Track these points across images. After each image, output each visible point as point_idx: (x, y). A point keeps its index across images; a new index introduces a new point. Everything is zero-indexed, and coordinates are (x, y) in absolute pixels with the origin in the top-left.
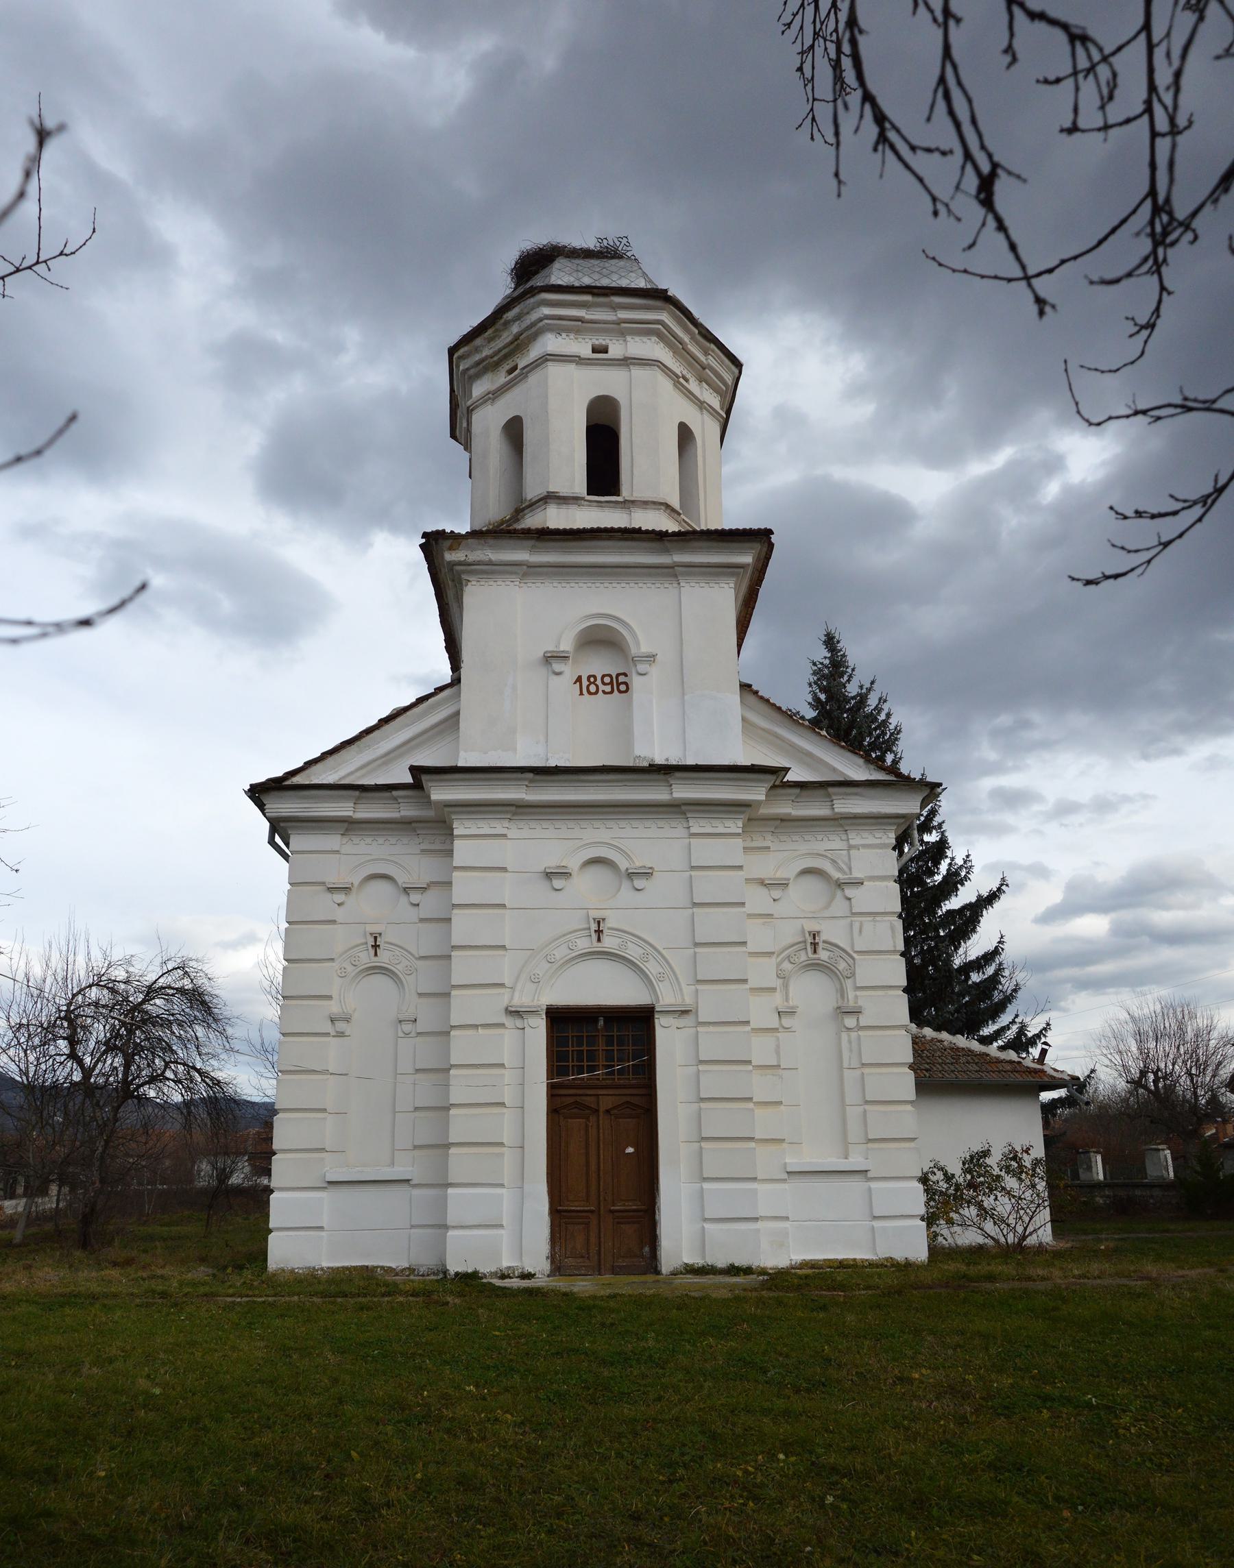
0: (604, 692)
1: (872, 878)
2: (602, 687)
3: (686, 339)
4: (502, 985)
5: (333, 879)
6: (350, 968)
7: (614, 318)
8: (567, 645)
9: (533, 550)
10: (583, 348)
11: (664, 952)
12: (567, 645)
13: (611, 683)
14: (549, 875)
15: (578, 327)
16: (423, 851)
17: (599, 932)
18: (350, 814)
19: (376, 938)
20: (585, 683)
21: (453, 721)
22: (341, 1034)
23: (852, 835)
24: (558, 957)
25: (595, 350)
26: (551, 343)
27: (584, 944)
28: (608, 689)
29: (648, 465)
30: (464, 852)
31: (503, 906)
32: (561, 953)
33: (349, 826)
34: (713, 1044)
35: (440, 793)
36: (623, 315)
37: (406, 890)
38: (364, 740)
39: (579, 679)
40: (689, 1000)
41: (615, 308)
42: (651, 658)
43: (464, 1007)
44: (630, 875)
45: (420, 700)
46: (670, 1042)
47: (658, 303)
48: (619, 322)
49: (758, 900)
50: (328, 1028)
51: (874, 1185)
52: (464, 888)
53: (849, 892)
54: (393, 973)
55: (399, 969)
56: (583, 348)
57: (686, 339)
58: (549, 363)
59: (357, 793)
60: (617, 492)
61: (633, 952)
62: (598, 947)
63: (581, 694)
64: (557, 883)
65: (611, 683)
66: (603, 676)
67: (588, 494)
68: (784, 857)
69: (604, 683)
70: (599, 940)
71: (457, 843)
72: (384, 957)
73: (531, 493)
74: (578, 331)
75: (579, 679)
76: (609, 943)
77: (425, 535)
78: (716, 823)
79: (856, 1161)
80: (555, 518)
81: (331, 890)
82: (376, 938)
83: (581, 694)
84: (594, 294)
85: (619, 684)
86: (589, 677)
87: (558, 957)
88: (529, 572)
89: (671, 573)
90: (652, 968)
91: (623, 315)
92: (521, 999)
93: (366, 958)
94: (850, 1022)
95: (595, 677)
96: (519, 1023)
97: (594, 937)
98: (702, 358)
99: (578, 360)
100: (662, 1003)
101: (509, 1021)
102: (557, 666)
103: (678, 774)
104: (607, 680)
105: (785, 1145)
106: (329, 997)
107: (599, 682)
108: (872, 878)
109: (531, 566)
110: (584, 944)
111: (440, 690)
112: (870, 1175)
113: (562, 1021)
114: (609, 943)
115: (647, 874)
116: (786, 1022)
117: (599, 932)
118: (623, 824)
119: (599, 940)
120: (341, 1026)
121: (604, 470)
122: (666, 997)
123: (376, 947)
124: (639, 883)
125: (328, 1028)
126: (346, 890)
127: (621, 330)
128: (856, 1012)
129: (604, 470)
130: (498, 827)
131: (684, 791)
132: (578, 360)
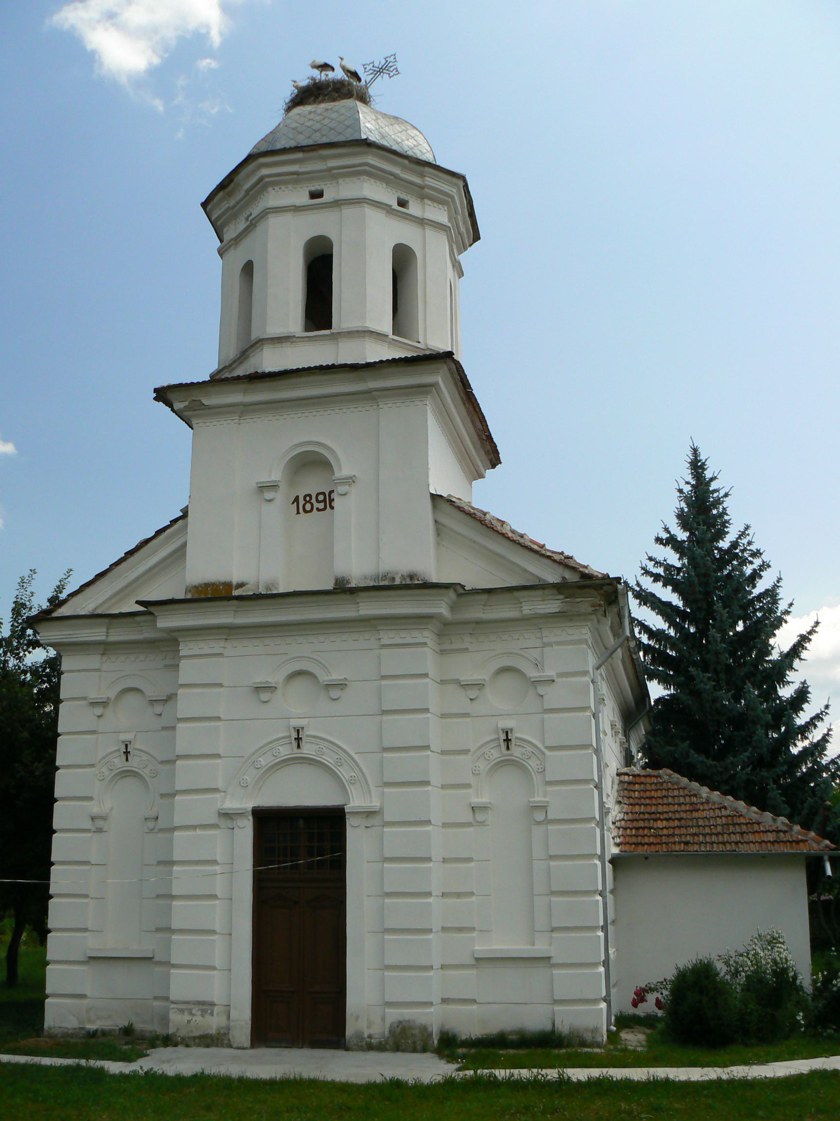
0: (318, 510)
2: (316, 505)
3: (397, 170)
4: (215, 790)
5: (93, 695)
6: (107, 772)
7: (324, 167)
8: (276, 475)
9: (245, 392)
10: (301, 197)
11: (356, 757)
12: (276, 475)
13: (324, 501)
14: (259, 689)
15: (297, 178)
16: (165, 666)
17: (298, 739)
18: (103, 638)
19: (126, 745)
20: (302, 502)
21: (181, 552)
22: (100, 830)
23: (545, 633)
24: (263, 763)
25: (316, 195)
26: (274, 198)
27: (286, 751)
28: (321, 506)
29: (363, 296)
30: (188, 670)
31: (218, 719)
32: (265, 761)
33: (106, 648)
34: (396, 840)
35: (166, 621)
36: (332, 163)
37: (152, 702)
38: (113, 572)
39: (297, 499)
40: (375, 804)
41: (325, 158)
42: (350, 480)
43: (186, 808)
44: (329, 686)
45: (159, 533)
46: (359, 843)
47: (365, 149)
48: (330, 169)
49: (459, 701)
50: (88, 824)
51: (556, 972)
52: (188, 703)
53: (541, 690)
54: (142, 776)
55: (146, 773)
56: (301, 197)
57: (397, 170)
58: (270, 215)
59: (106, 620)
60: (329, 326)
61: (328, 759)
62: (297, 753)
63: (298, 513)
64: (264, 696)
65: (324, 501)
66: (318, 495)
67: (307, 329)
68: (476, 662)
69: (318, 501)
70: (299, 747)
71: (183, 663)
72: (135, 763)
73: (254, 336)
74: (296, 182)
75: (297, 499)
76: (308, 749)
77: (156, 390)
78: (403, 634)
79: (541, 947)
80: (270, 361)
81: (94, 704)
82: (126, 745)
83: (298, 513)
84: (303, 151)
85: (327, 501)
86: (305, 497)
87: (263, 763)
88: (245, 410)
89: (369, 396)
90: (345, 773)
91: (332, 163)
92: (231, 804)
93: (119, 762)
94: (539, 816)
95: (310, 496)
96: (230, 824)
97: (295, 744)
98: (417, 180)
99: (296, 209)
100: (352, 804)
101: (223, 823)
102: (268, 495)
103: (362, 594)
104: (321, 498)
105: (475, 934)
106: (90, 799)
107: (313, 500)
109: (246, 405)
110: (286, 751)
111: (174, 522)
112: (553, 961)
113: (270, 824)
114: (308, 749)
115: (342, 685)
116: (480, 817)
117: (298, 739)
118: (322, 638)
119: (299, 747)
120: (100, 823)
121: (319, 309)
122: (355, 802)
123: (127, 753)
124: (334, 693)
125: (88, 824)
126: (104, 704)
127: (333, 175)
128: (543, 808)
129: (319, 309)
130: (215, 646)
131: (368, 608)
132: (296, 209)
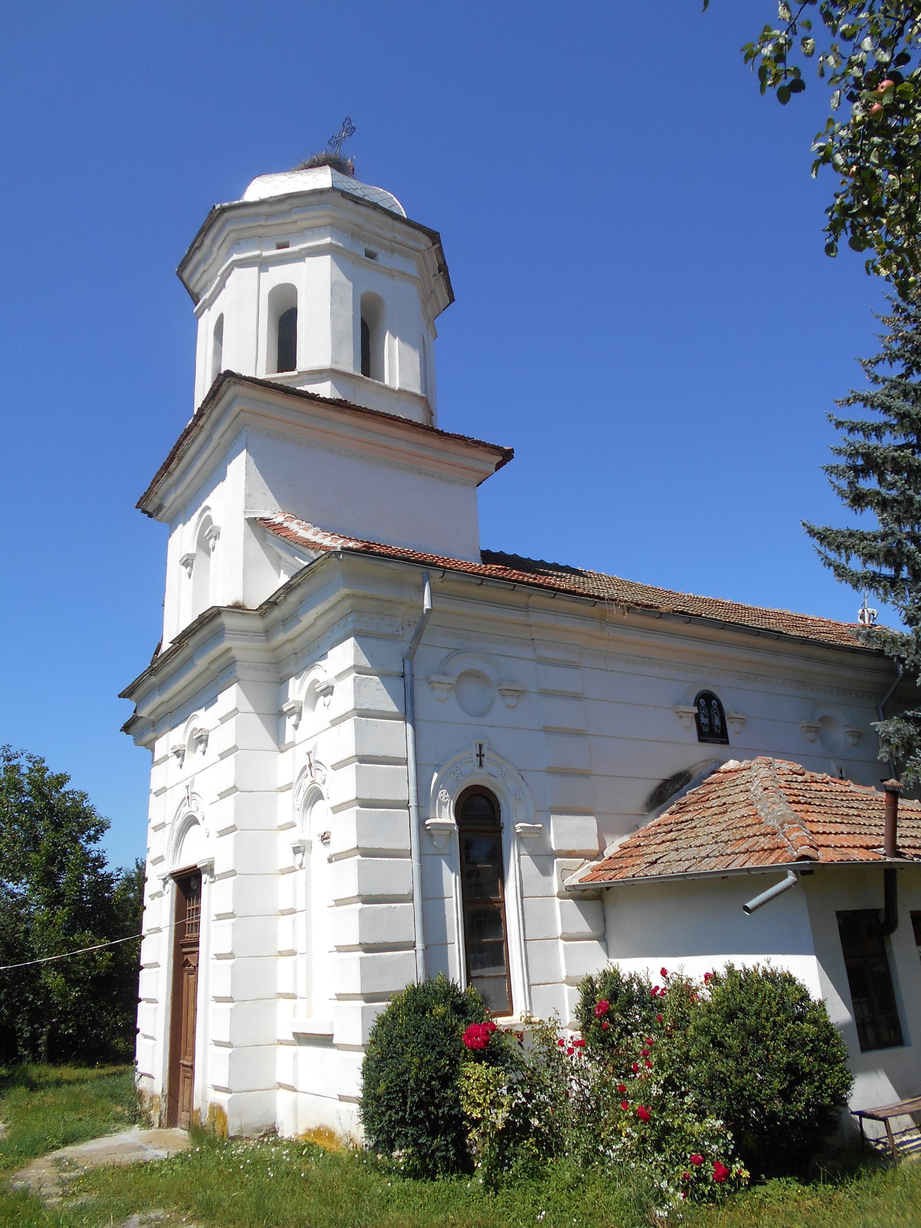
1: (340, 676)
32: (178, 824)
108: (340, 676)
